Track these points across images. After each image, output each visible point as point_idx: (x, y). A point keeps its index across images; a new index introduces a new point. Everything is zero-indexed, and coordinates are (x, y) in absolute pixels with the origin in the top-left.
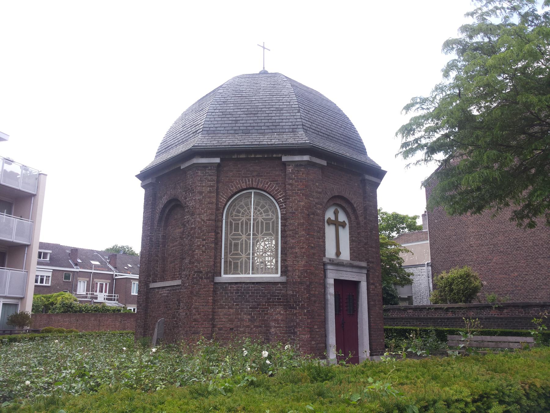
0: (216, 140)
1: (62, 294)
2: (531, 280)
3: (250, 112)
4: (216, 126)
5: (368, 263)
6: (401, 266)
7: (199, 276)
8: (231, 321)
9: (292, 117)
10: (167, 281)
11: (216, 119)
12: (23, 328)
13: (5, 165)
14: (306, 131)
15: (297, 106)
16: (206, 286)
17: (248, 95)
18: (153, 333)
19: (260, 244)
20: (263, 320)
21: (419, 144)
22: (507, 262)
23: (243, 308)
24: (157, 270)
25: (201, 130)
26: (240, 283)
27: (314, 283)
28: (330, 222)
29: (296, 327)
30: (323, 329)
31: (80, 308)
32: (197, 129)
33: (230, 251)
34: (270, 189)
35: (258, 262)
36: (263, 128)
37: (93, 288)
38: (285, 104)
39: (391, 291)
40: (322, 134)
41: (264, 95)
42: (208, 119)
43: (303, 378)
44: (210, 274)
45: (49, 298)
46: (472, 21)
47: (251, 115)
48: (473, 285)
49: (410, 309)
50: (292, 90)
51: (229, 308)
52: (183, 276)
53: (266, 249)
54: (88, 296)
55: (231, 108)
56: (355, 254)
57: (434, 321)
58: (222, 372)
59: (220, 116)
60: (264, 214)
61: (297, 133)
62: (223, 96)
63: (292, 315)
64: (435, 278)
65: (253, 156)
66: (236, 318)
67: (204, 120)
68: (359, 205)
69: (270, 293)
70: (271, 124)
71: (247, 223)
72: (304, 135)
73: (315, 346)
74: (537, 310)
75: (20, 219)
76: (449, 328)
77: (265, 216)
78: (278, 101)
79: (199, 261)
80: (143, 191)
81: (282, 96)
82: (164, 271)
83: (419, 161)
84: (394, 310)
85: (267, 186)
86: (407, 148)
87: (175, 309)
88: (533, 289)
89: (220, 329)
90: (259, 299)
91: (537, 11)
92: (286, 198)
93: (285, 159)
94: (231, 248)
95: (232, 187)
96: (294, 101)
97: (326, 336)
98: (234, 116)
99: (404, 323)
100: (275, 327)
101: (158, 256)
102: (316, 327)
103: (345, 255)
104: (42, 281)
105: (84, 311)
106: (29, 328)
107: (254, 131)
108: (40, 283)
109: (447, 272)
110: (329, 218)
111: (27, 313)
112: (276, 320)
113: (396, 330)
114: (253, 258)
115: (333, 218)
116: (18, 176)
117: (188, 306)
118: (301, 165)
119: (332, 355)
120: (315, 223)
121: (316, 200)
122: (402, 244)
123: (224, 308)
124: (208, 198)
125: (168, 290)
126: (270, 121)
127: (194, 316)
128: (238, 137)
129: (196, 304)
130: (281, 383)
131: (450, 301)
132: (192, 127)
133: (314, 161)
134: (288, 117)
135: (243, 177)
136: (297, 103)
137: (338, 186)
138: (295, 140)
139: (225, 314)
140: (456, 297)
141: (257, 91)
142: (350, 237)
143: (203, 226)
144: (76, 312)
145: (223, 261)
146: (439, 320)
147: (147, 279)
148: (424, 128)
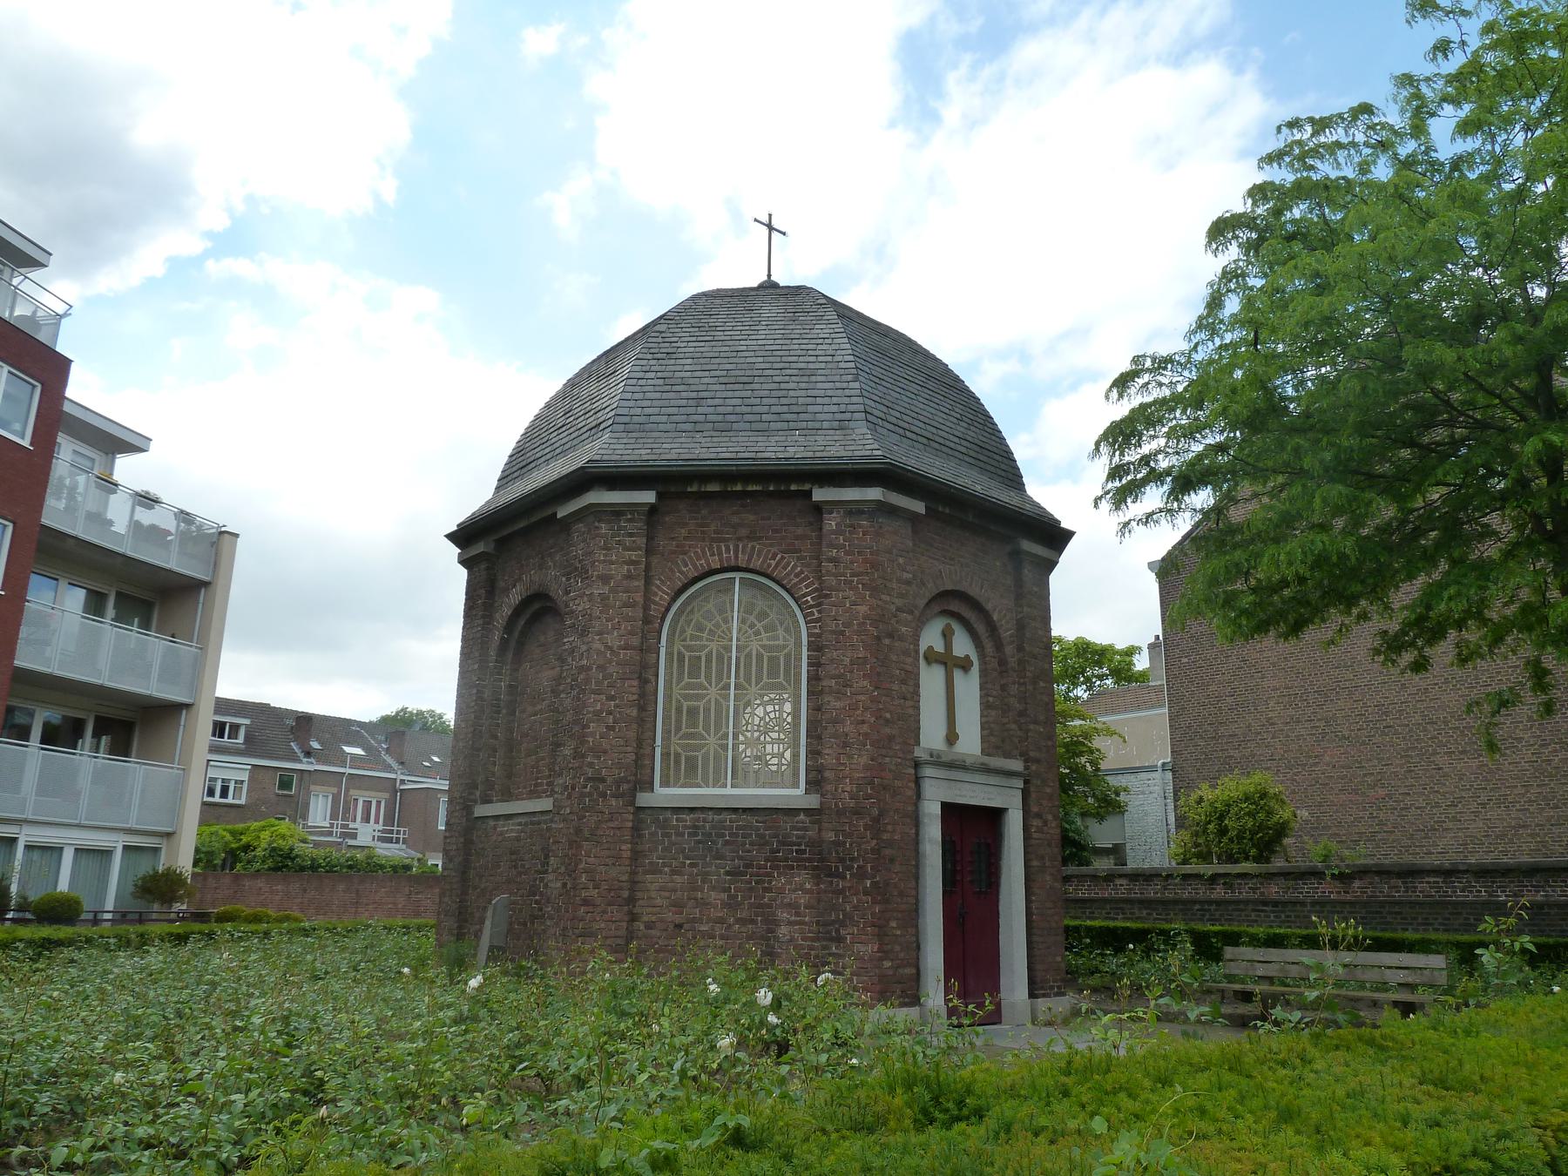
0: (646, 446)
1: (273, 826)
2: (1417, 808)
3: (732, 380)
4: (647, 411)
5: (1026, 761)
6: (1098, 770)
7: (597, 789)
8: (678, 905)
9: (839, 392)
10: (518, 799)
11: (649, 395)
12: (171, 907)
13: (138, 508)
14: (873, 426)
15: (852, 365)
16: (615, 816)
17: (729, 338)
18: (481, 930)
19: (753, 714)
20: (760, 906)
21: (1153, 470)
22: (1360, 763)
23: (708, 874)
24: (493, 774)
25: (610, 422)
26: (703, 809)
27: (892, 813)
28: (932, 657)
29: (843, 924)
30: (912, 930)
31: (313, 860)
32: (600, 420)
33: (678, 729)
34: (781, 572)
35: (746, 757)
36: (764, 417)
37: (347, 810)
38: (820, 359)
39: (1073, 832)
40: (914, 436)
41: (768, 337)
42: (628, 396)
43: (889, 1113)
44: (626, 786)
45: (241, 834)
46: (1282, 175)
47: (736, 387)
48: (1275, 819)
49: (1121, 876)
50: (840, 325)
51: (673, 872)
52: (556, 790)
53: (768, 723)
54: (335, 830)
55: (687, 368)
56: (993, 739)
57: (1185, 906)
58: (650, 1069)
59: (657, 389)
60: (763, 635)
61: (850, 432)
62: (667, 340)
63: (833, 892)
64: (1181, 802)
65: (739, 488)
66: (689, 899)
67: (618, 397)
68: (1005, 615)
69: (776, 836)
70: (785, 409)
71: (720, 658)
72: (870, 437)
73: (891, 973)
74: (1434, 882)
75: (171, 641)
76: (1222, 925)
77: (769, 639)
78: (804, 352)
79: (599, 752)
80: (462, 574)
81: (814, 341)
82: (510, 776)
83: (1153, 513)
84: (1081, 878)
85: (773, 563)
86: (1124, 481)
87: (536, 871)
88: (1424, 830)
89: (649, 926)
90: (749, 851)
91: (1436, 151)
92: (821, 595)
93: (820, 494)
94: (679, 721)
95: (686, 565)
96: (843, 352)
97: (918, 947)
98: (693, 388)
99: (1109, 913)
100: (790, 923)
101: (496, 737)
102: (893, 924)
103: (970, 743)
104: (224, 793)
105: (323, 867)
106: (184, 907)
107: (742, 426)
108: (221, 797)
109: (1214, 787)
110: (931, 648)
111: (181, 872)
112: (792, 906)
113: (1089, 929)
114: (735, 747)
115: (939, 647)
116: (169, 538)
117: (570, 864)
118: (861, 512)
119: (935, 995)
120: (894, 658)
121: (900, 602)
122: (1100, 715)
123: (661, 872)
124: (624, 592)
125: (520, 824)
126: (784, 401)
127: (583, 891)
128: (703, 440)
129: (589, 860)
130: (824, 1132)
131: (1219, 858)
132: (587, 416)
133: (894, 503)
134: (830, 393)
135: (713, 540)
136: (851, 358)
137: (952, 568)
138: (847, 448)
139: (662, 889)
140: (1235, 848)
141: (753, 328)
142: (981, 697)
143: (610, 661)
144: (302, 869)
145: (658, 751)
146: (1197, 907)
147: (470, 794)
148: (1166, 429)
